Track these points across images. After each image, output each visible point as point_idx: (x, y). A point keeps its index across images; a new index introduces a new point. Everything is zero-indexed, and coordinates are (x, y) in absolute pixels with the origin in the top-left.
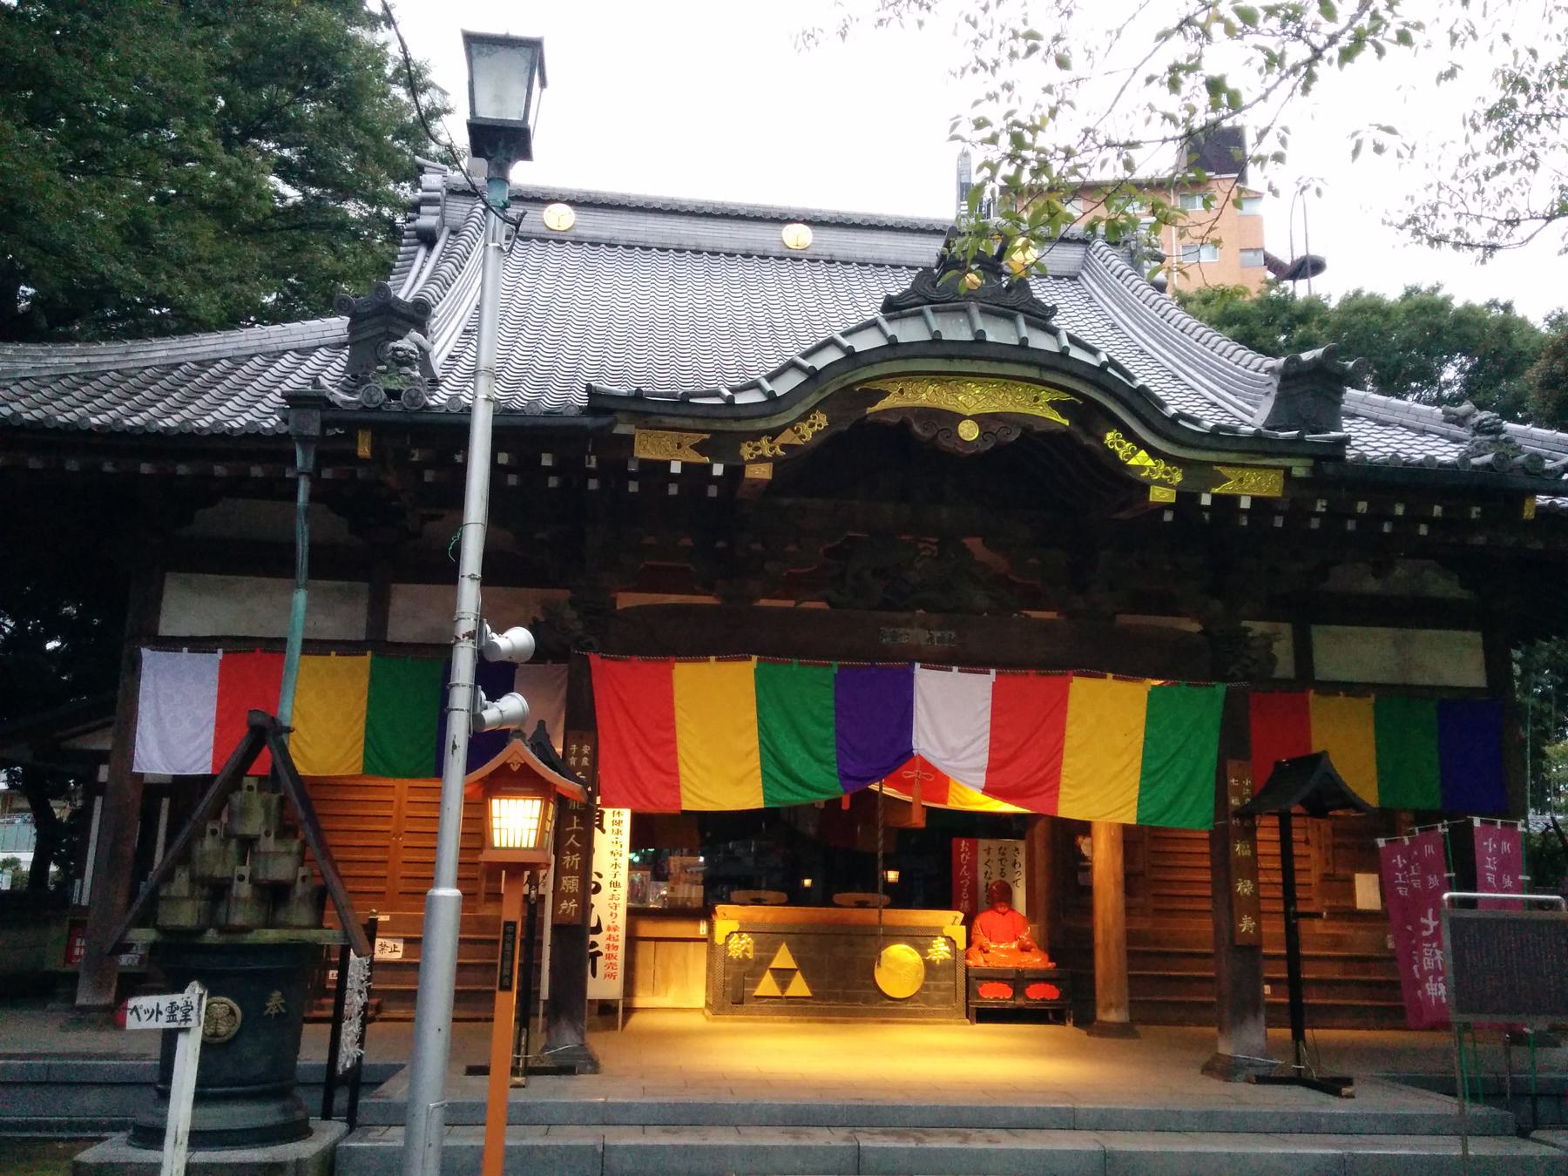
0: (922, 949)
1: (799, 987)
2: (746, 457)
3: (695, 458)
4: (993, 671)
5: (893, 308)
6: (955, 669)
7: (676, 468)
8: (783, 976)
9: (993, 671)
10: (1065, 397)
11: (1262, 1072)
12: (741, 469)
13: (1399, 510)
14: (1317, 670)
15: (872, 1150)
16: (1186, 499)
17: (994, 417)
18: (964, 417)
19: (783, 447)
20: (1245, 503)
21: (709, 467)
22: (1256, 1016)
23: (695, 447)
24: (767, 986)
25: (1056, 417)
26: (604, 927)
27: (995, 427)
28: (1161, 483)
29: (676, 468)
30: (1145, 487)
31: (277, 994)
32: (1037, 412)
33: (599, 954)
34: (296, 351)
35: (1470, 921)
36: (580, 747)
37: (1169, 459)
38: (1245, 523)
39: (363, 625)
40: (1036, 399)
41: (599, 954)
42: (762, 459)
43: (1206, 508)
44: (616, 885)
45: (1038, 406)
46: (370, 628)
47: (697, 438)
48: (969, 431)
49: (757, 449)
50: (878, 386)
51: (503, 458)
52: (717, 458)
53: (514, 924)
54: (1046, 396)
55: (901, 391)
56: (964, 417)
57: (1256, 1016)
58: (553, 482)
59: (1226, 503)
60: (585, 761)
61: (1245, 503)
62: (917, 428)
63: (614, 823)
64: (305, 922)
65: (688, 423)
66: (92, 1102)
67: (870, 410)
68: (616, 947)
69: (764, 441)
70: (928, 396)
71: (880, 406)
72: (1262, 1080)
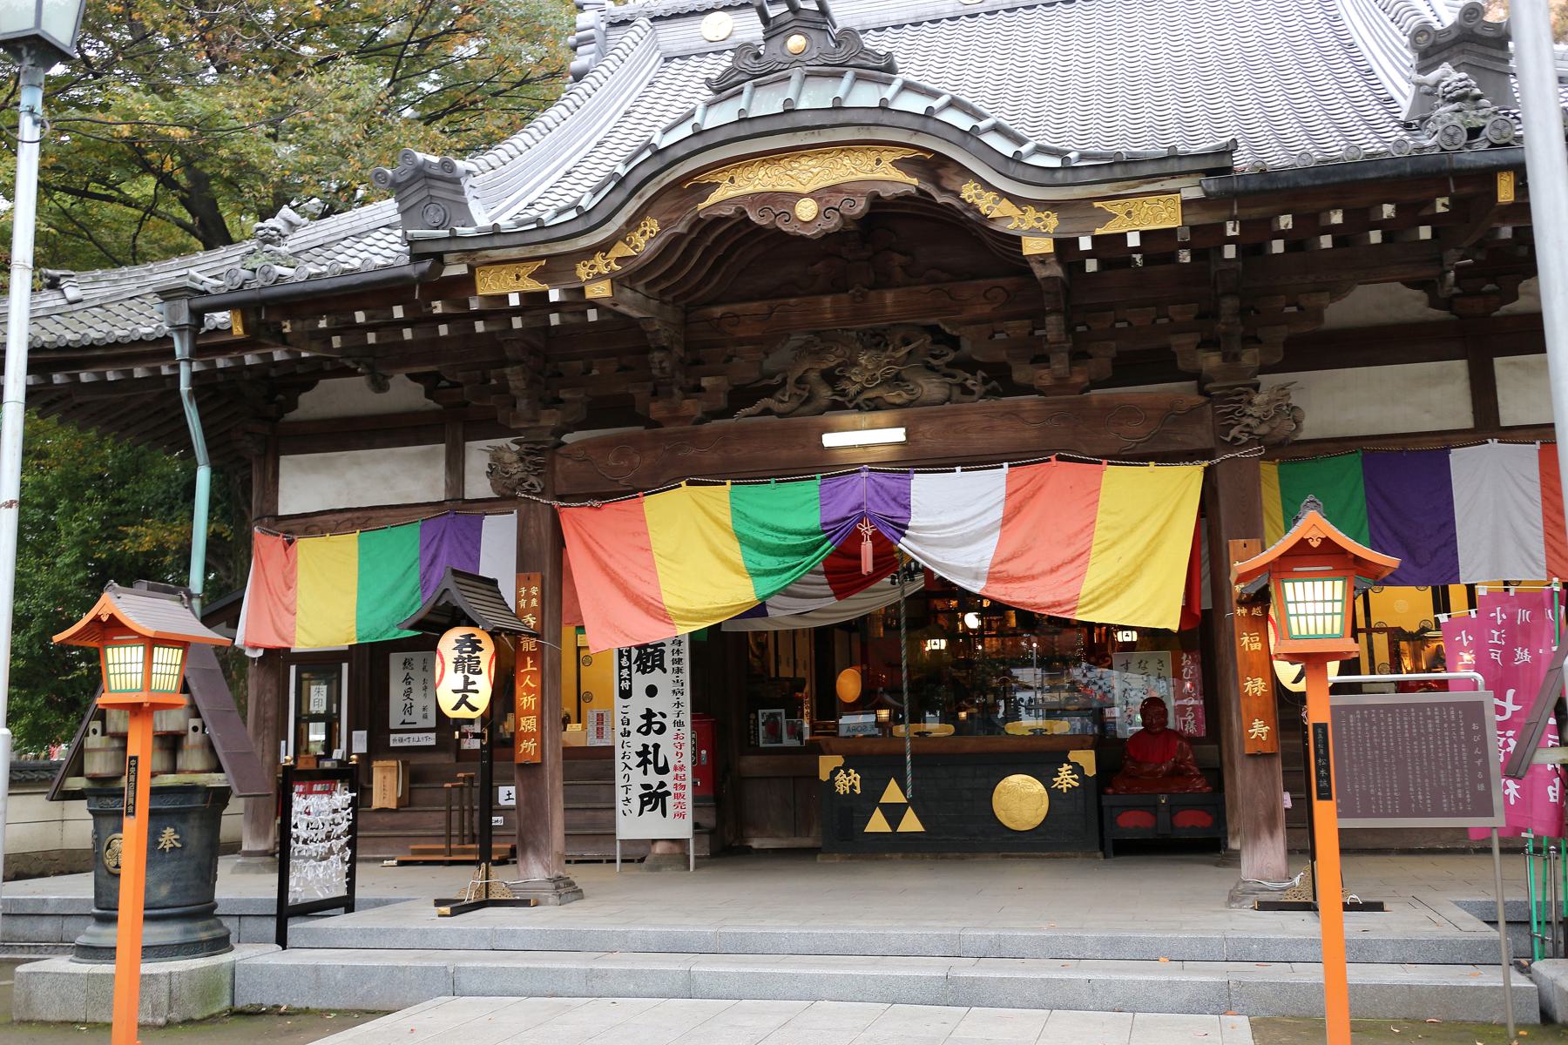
0: (1046, 779)
1: (911, 823)
2: (584, 278)
3: (534, 286)
4: (1006, 465)
5: (723, 88)
6: (1152, 464)
7: (514, 301)
8: (894, 813)
9: (1006, 465)
10: (909, 154)
11: (1265, 897)
12: (582, 291)
13: (1337, 218)
14: (1502, 412)
15: (701, 973)
16: (1065, 246)
17: (834, 189)
18: (800, 196)
19: (618, 260)
20: (1134, 241)
21: (546, 294)
22: (1272, 834)
23: (532, 276)
24: (878, 823)
25: (899, 176)
26: (671, 767)
27: (835, 201)
28: (1034, 232)
29: (514, 301)
30: (1016, 241)
31: (169, 831)
32: (879, 175)
33: (668, 793)
34: (386, 226)
35: (1448, 705)
36: (528, 588)
37: (1039, 205)
38: (1188, 260)
39: (443, 486)
40: (878, 161)
41: (668, 793)
42: (599, 277)
43: (1135, 250)
44: (679, 724)
45: (884, 174)
46: (448, 489)
47: (534, 267)
48: (806, 210)
49: (592, 267)
50: (705, 179)
51: (1523, 251)
52: (553, 282)
53: (1320, 798)
54: (889, 157)
55: (732, 180)
56: (800, 196)
57: (1272, 834)
58: (517, 323)
59: (1110, 246)
60: (534, 602)
61: (1134, 241)
62: (753, 217)
63: (674, 661)
64: (198, 767)
65: (515, 253)
66: (47, 928)
67: (701, 206)
68: (683, 787)
69: (598, 256)
70: (762, 180)
71: (714, 198)
72: (1264, 906)
